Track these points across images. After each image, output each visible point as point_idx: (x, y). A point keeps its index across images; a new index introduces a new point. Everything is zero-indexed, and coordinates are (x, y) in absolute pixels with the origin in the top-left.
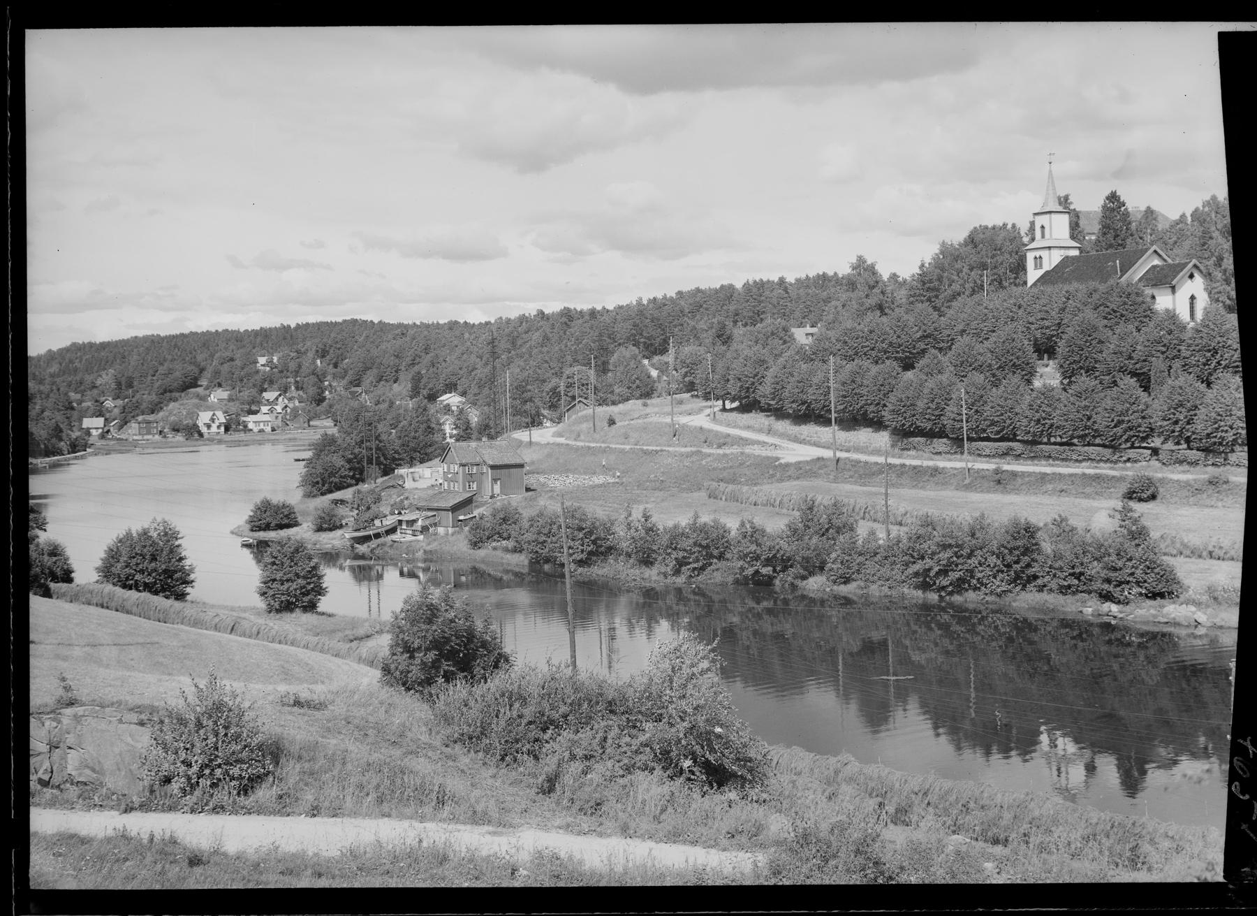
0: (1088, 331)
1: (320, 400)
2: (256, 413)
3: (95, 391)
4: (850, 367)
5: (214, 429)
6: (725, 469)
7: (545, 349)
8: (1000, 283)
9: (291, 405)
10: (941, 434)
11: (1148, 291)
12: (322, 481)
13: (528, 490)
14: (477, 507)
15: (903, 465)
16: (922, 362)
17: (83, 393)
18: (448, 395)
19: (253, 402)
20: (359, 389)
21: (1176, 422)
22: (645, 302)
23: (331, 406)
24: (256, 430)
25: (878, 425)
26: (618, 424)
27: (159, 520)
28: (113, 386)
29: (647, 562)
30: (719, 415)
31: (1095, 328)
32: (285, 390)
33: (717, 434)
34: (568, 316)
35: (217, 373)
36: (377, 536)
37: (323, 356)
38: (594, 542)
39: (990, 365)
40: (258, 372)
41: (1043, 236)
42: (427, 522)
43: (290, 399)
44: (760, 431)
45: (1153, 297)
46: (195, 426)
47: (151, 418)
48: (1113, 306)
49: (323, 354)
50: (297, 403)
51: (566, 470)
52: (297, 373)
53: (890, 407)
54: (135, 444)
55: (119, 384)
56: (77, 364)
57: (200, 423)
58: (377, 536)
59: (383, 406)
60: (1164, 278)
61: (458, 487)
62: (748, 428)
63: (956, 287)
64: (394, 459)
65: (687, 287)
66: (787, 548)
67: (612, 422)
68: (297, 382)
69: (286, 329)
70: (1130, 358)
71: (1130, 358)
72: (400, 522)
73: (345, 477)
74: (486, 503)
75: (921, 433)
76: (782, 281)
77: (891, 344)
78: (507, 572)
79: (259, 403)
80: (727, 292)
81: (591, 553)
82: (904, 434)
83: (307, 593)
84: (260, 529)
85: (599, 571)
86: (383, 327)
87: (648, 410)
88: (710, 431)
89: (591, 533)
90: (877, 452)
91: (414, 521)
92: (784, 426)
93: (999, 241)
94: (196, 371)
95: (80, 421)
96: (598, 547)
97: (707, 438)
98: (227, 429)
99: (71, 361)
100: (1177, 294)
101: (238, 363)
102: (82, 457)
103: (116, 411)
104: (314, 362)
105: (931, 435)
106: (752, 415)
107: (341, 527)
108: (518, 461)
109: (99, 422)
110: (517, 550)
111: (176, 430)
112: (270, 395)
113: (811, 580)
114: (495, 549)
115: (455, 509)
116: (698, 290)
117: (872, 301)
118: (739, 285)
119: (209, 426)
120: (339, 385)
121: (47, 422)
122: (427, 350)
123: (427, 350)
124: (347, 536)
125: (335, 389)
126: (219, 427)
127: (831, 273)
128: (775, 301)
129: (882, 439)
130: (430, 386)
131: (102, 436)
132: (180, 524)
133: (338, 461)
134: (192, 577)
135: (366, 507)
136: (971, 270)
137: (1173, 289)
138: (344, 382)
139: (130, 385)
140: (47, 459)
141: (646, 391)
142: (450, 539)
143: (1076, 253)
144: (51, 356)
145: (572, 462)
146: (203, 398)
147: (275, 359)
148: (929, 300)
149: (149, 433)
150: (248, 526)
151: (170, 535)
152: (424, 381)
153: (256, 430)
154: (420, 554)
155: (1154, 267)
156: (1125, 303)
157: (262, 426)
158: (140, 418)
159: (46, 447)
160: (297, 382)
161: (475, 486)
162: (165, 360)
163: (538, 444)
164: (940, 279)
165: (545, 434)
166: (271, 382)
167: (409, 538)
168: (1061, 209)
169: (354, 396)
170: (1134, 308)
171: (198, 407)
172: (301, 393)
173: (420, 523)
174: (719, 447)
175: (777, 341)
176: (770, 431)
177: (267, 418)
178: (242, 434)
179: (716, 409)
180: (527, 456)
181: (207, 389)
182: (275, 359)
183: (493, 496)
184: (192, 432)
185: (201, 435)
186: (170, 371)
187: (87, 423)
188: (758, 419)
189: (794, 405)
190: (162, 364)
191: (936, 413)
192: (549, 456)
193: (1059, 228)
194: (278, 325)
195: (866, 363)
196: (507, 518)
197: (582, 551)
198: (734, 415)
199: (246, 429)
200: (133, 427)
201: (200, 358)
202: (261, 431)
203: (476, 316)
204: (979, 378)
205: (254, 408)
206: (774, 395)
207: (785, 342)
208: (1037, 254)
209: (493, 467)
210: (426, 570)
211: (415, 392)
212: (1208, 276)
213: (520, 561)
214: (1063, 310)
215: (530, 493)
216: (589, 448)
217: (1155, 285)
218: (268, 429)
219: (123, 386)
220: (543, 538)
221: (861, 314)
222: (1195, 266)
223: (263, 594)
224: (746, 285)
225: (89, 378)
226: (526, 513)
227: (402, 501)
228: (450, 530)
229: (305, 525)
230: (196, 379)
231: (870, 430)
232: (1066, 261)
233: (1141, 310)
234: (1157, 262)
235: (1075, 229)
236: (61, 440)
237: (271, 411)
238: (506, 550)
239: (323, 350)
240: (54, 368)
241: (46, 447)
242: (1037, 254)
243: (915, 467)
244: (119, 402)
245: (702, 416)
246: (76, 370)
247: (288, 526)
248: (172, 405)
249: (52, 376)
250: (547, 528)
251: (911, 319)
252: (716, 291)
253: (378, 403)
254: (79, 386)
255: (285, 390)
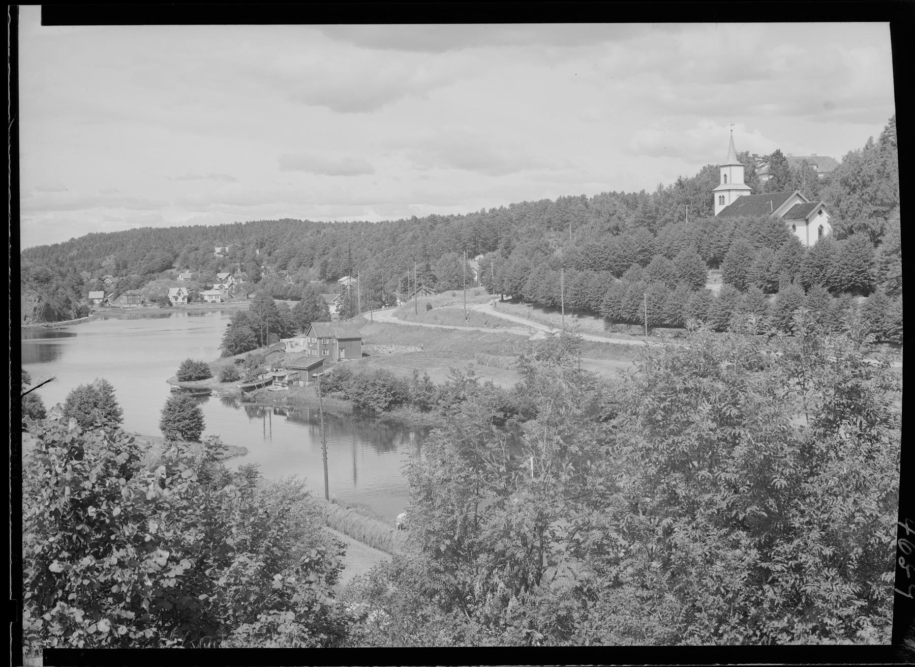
0: (743, 251)
1: (257, 279)
2: (210, 288)
3: (101, 271)
4: (580, 274)
5: (180, 300)
6: (491, 344)
7: (413, 246)
8: (699, 213)
9: (236, 283)
10: (638, 322)
11: (789, 223)
12: (236, 345)
13: (364, 355)
14: (328, 367)
15: (608, 344)
16: (628, 272)
17: (92, 271)
18: (346, 278)
19: (208, 280)
20: (285, 272)
21: (784, 318)
22: (487, 211)
23: (265, 284)
24: (209, 301)
25: (596, 314)
26: (434, 309)
27: (100, 379)
28: (114, 267)
29: (425, 408)
30: (498, 304)
31: (747, 250)
32: (233, 271)
33: (494, 318)
34: (434, 220)
35: (186, 259)
36: (259, 386)
37: (261, 247)
38: (394, 395)
39: (674, 275)
40: (214, 258)
41: (725, 182)
42: (292, 378)
43: (236, 278)
44: (523, 316)
45: (794, 227)
46: (167, 298)
47: (137, 292)
48: (763, 233)
49: (261, 245)
50: (241, 282)
51: (391, 342)
52: (242, 259)
53: (605, 302)
54: (124, 311)
55: (118, 265)
56: (90, 250)
57: (170, 297)
58: (259, 386)
59: (301, 284)
60: (802, 214)
61: (316, 353)
62: (516, 314)
63: (668, 216)
64: (289, 329)
65: (518, 201)
66: (514, 402)
67: (429, 307)
68: (242, 266)
69: (238, 225)
70: (768, 271)
71: (768, 271)
72: (274, 377)
73: (252, 342)
74: (334, 364)
75: (623, 321)
76: (583, 198)
77: (619, 256)
78: (341, 413)
79: (213, 282)
80: (544, 205)
81: (391, 402)
82: (614, 321)
83: (191, 429)
84: (185, 380)
85: (397, 414)
86: (308, 225)
87: (455, 299)
88: (490, 316)
89: (391, 389)
90: (596, 333)
91: (283, 377)
92: (538, 313)
93: (698, 184)
94: (171, 257)
95: (88, 293)
96: (397, 399)
97: (487, 321)
98: (189, 300)
99: (86, 248)
100: (810, 225)
101: (201, 252)
102: (85, 321)
103: (113, 286)
104: (254, 252)
105: (630, 322)
106: (519, 305)
107: (239, 379)
108: (357, 336)
109: (101, 294)
110: (346, 398)
111: (153, 301)
112: (222, 275)
113: (528, 422)
114: (333, 397)
115: (310, 369)
116: (525, 203)
117: (612, 224)
118: (554, 199)
119: (176, 298)
120: (272, 269)
121: (60, 296)
122: (333, 244)
123: (333, 244)
124: (239, 386)
125: (269, 272)
126: (183, 299)
127: (619, 192)
128: (576, 213)
129: (600, 324)
130: (334, 271)
131: (102, 305)
132: (111, 382)
133: (246, 331)
134: (121, 417)
135: (256, 366)
136: (679, 204)
137: (807, 222)
138: (276, 266)
139: (125, 267)
140: (60, 323)
141: (461, 282)
142: (307, 389)
143: (748, 194)
144: (44, 252)
145: (398, 338)
146: (174, 278)
147: (227, 249)
148: (649, 225)
149: (134, 303)
150: (177, 378)
151: (107, 389)
152: (329, 267)
153: (209, 301)
154: (285, 400)
155: (796, 205)
156: (771, 232)
157: (214, 298)
158: (129, 292)
159: (59, 313)
160: (242, 266)
161: (328, 353)
162: (151, 248)
163: (377, 322)
164: (657, 210)
165: (384, 315)
166: (224, 266)
167: (280, 388)
168: (738, 163)
169: (281, 276)
170: (778, 236)
171: (169, 284)
172: (244, 273)
173: (287, 378)
174: (494, 327)
175: (539, 254)
176: (529, 317)
177: (218, 292)
178: (200, 304)
179: (497, 300)
180: (364, 332)
181: (178, 270)
182: (227, 249)
183: (340, 359)
184: (165, 301)
185: (171, 304)
186: (153, 258)
187: (92, 295)
188: (522, 308)
189: (544, 300)
190: (149, 251)
191: (633, 308)
192: (382, 331)
193: (736, 176)
194: (233, 223)
195: (590, 272)
196: (343, 376)
197: (386, 401)
198: (508, 305)
199: (203, 300)
200: (123, 299)
201: (176, 247)
202: (213, 302)
203: (374, 217)
204: (662, 285)
205: (209, 285)
206: (533, 290)
207: (546, 254)
208: (722, 194)
209: (340, 340)
210: (291, 410)
211: (323, 274)
212: (831, 213)
213: (348, 405)
214: (732, 235)
215: (365, 358)
216: (408, 326)
217: (795, 219)
218: (219, 300)
219: (121, 267)
220: (361, 391)
221: (601, 234)
222: (823, 205)
223: (164, 429)
224: (559, 200)
225: (97, 261)
226: (356, 372)
227: (279, 362)
228: (307, 383)
229: (216, 378)
230: (171, 263)
231: (593, 317)
232: (741, 199)
233: (782, 236)
234: (799, 202)
235: (750, 177)
236: (70, 309)
237: (221, 287)
238: (340, 398)
239: (262, 243)
240: (74, 253)
241: (59, 313)
242: (722, 194)
243: (615, 345)
244: (116, 279)
245: (487, 306)
246: (89, 254)
247: (204, 378)
248: (151, 283)
249: (72, 259)
250: (365, 384)
251: (633, 238)
252: (535, 204)
253: (298, 282)
254: (91, 267)
255: (233, 271)
